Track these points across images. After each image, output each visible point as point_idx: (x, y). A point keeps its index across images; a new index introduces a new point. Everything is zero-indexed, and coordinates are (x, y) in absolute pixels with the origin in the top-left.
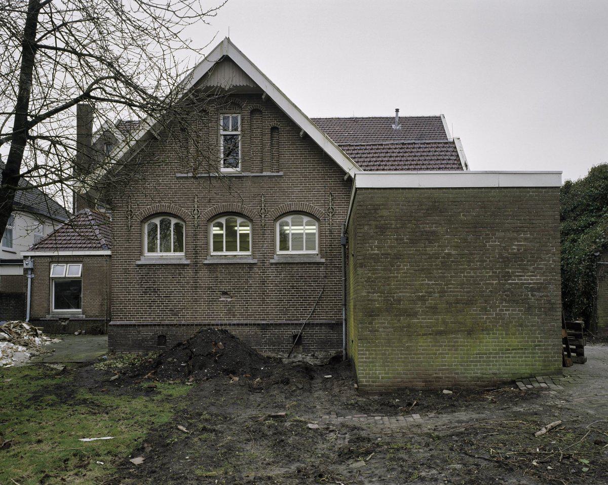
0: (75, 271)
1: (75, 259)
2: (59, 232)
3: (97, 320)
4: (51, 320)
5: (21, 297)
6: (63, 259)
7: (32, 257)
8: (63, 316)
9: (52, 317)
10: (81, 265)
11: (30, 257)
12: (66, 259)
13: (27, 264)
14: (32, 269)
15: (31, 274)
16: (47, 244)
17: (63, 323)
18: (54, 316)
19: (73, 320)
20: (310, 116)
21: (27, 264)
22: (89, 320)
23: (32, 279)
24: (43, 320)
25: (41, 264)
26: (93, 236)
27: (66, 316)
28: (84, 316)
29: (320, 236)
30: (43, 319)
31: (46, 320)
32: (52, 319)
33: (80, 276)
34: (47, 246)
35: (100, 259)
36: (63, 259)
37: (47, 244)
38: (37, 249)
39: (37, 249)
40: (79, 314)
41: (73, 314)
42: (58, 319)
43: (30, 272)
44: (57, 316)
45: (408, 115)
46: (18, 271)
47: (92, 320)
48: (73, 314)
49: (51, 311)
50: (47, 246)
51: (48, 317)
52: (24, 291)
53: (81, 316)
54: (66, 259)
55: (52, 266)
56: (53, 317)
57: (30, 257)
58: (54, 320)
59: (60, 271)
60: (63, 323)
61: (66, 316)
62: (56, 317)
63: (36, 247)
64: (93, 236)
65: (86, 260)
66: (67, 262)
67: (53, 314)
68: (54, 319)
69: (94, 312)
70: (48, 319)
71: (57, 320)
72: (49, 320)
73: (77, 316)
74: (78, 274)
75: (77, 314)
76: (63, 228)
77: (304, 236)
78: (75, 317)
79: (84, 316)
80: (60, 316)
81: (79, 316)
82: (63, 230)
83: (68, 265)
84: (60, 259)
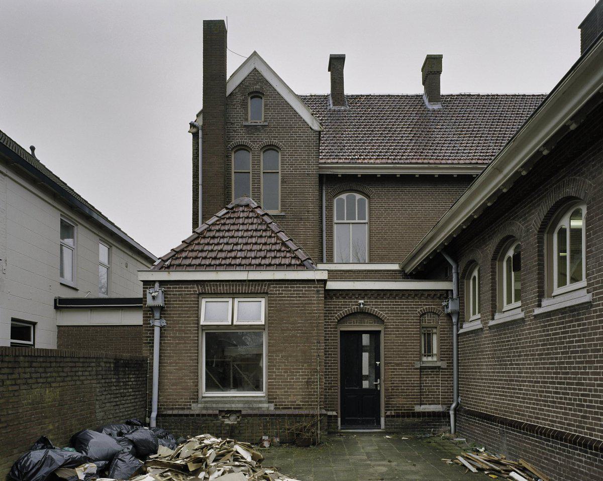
0: (252, 312)
1: (252, 289)
2: (204, 237)
3: (301, 416)
4: (204, 415)
5: (141, 367)
6: (226, 289)
7: (162, 283)
8: (227, 407)
9: (204, 408)
10: (263, 300)
11: (157, 285)
12: (234, 289)
13: (154, 298)
14: (161, 309)
15: (161, 318)
16: (186, 258)
17: (227, 421)
18: (208, 405)
19: (250, 415)
20: (579, 56)
21: (154, 298)
22: (284, 415)
23: (161, 328)
24: (187, 415)
25: (180, 298)
26: (276, 244)
27: (234, 406)
28: (272, 407)
29: (587, 231)
30: (186, 412)
31: (192, 415)
32: (204, 412)
33: (263, 323)
34: (187, 262)
35: (304, 288)
36: (226, 289)
37: (186, 258)
38: (168, 267)
39: (168, 267)
40: (260, 402)
41: (247, 402)
42: (217, 412)
43: (157, 315)
44: (214, 405)
45: (455, 92)
46: (135, 319)
47: (289, 415)
48: (247, 401)
49: (200, 396)
50: (187, 262)
51: (196, 408)
52: (145, 353)
53: (266, 405)
54: (234, 289)
55: (203, 302)
56: (206, 408)
57: (157, 285)
58: (210, 415)
59: (216, 313)
60: (227, 421)
61: (233, 406)
62: (212, 408)
63: (167, 263)
64: (276, 244)
65: (272, 289)
66: (233, 295)
67: (206, 402)
68: (210, 412)
69: (291, 399)
70: (197, 412)
71: (216, 416)
72: (198, 415)
73: (255, 405)
74: (259, 319)
75: (255, 402)
76: (210, 230)
77: (357, 218)
78: (253, 409)
79: (272, 407)
80: (221, 405)
81: (260, 405)
82: (212, 234)
83: (236, 300)
84: (220, 289)
